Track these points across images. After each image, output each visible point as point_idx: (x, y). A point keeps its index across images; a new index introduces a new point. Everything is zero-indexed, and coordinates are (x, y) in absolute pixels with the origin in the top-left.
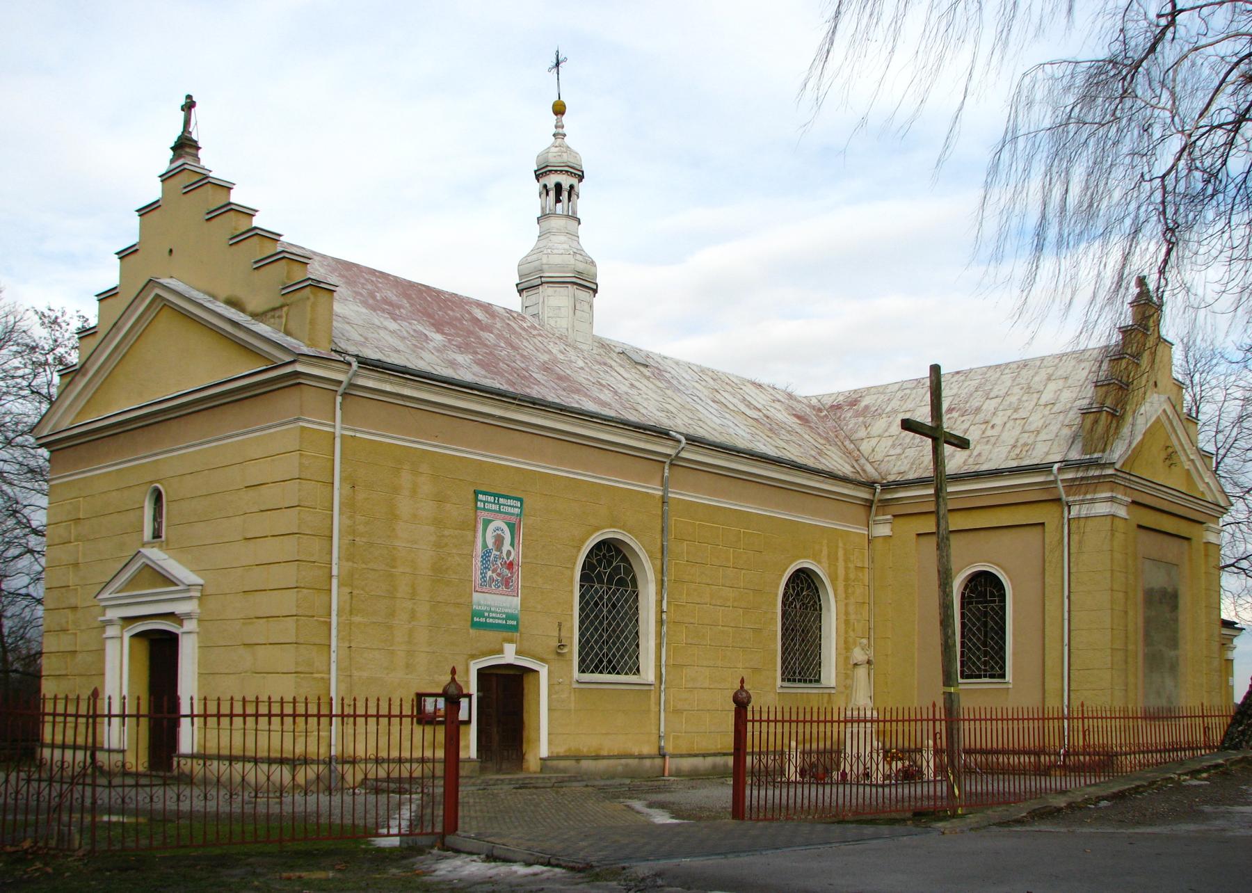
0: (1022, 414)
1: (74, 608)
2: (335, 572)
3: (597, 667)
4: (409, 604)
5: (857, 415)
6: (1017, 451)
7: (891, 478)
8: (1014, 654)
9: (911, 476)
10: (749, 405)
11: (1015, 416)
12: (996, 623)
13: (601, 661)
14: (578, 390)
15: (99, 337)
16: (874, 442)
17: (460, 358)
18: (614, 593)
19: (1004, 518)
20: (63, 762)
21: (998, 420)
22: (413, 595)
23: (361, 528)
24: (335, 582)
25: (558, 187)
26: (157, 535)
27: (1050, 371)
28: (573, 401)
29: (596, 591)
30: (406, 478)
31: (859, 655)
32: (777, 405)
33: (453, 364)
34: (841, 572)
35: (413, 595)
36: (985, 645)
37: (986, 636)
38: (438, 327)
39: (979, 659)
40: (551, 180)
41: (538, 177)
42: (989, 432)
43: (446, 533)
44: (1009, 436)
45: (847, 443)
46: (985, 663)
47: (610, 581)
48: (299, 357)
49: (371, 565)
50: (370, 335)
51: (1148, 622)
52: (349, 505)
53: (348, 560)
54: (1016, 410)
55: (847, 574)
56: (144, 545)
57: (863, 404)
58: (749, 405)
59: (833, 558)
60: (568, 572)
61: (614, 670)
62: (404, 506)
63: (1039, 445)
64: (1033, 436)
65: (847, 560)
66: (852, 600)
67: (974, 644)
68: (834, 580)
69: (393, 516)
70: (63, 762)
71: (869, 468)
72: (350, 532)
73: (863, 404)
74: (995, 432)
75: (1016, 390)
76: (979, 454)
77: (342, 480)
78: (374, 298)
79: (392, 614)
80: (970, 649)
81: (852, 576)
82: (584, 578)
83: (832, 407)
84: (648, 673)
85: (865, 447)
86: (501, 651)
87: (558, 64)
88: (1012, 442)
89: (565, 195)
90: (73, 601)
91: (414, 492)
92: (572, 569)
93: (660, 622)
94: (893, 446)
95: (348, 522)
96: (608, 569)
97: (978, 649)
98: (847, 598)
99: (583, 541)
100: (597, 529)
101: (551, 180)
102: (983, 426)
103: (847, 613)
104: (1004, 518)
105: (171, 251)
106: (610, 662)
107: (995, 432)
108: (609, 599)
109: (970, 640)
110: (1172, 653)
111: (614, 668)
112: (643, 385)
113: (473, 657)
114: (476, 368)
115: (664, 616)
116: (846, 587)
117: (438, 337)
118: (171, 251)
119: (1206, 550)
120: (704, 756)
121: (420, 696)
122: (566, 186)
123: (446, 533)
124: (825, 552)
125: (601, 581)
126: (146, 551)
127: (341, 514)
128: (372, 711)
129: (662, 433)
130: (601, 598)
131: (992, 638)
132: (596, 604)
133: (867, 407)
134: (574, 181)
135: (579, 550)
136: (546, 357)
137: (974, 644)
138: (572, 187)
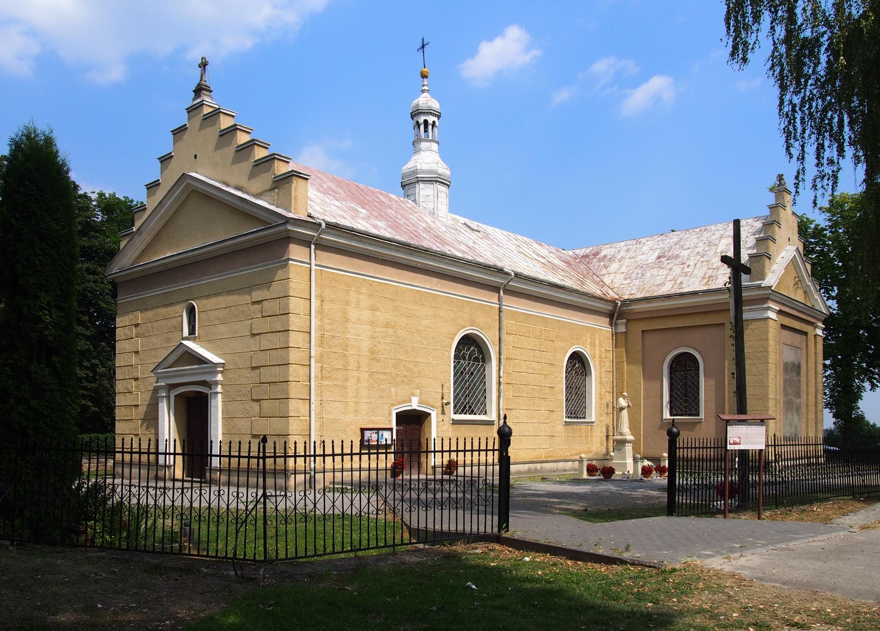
0: (706, 258)
1: (136, 379)
2: (313, 354)
3: (463, 411)
4: (355, 374)
5: (600, 260)
6: (706, 280)
7: (626, 297)
8: (705, 401)
9: (639, 296)
10: (538, 255)
11: (702, 260)
12: (693, 383)
13: (465, 407)
14: (443, 242)
15: (148, 213)
16: (612, 277)
17: (379, 223)
18: (472, 366)
19: (699, 321)
20: (442, 509)
21: (692, 263)
22: (358, 369)
23: (327, 327)
24: (313, 360)
25: (426, 122)
26: (192, 331)
27: (721, 232)
28: (446, 250)
29: (462, 365)
30: (353, 296)
31: (623, 402)
32: (552, 255)
33: (375, 226)
34: (597, 353)
35: (358, 369)
36: (686, 396)
37: (686, 389)
38: (363, 205)
39: (681, 404)
40: (421, 119)
41: (412, 117)
42: (686, 270)
43: (377, 330)
44: (699, 273)
45: (595, 277)
46: (685, 407)
47: (470, 359)
48: (288, 220)
49: (334, 350)
50: (326, 209)
51: (785, 381)
52: (321, 312)
53: (320, 346)
54: (703, 256)
55: (601, 354)
56: (184, 339)
57: (602, 254)
58: (538, 255)
59: (593, 344)
60: (447, 354)
61: (472, 412)
62: (353, 313)
63: (720, 277)
64: (715, 272)
65: (600, 346)
66: (604, 370)
67: (679, 396)
68: (594, 357)
69: (346, 320)
70: (442, 509)
71: (610, 292)
72: (321, 328)
73: (602, 254)
74: (690, 269)
75: (701, 244)
76: (681, 283)
77: (317, 297)
78: (323, 187)
79: (346, 380)
80: (676, 399)
81: (604, 356)
82: (456, 357)
83: (583, 256)
84: (702, 416)
85: (607, 280)
86: (410, 401)
87: (423, 47)
88: (702, 275)
89: (430, 127)
90: (135, 375)
91: (358, 305)
92: (449, 352)
93: (499, 383)
94: (625, 279)
95: (320, 323)
96: (471, 350)
97: (681, 399)
98: (601, 368)
99: (455, 335)
100: (463, 327)
101: (421, 119)
102: (682, 266)
103: (601, 378)
104: (699, 321)
105: (196, 157)
106: (470, 407)
107: (690, 269)
108: (469, 369)
109: (676, 393)
110: (798, 401)
111: (472, 411)
112: (479, 241)
113: (393, 405)
114: (390, 230)
115: (501, 380)
116: (600, 362)
117: (364, 211)
118: (196, 157)
119: (815, 339)
120: (524, 463)
121: (363, 430)
122: (430, 122)
123: (377, 330)
124: (589, 341)
125: (464, 359)
126: (185, 342)
127: (316, 318)
128: (461, 447)
129: (500, 271)
130: (465, 369)
131: (690, 392)
132: (462, 373)
133: (605, 256)
134: (436, 119)
135: (453, 340)
136: (424, 225)
137: (679, 396)
138: (434, 122)
